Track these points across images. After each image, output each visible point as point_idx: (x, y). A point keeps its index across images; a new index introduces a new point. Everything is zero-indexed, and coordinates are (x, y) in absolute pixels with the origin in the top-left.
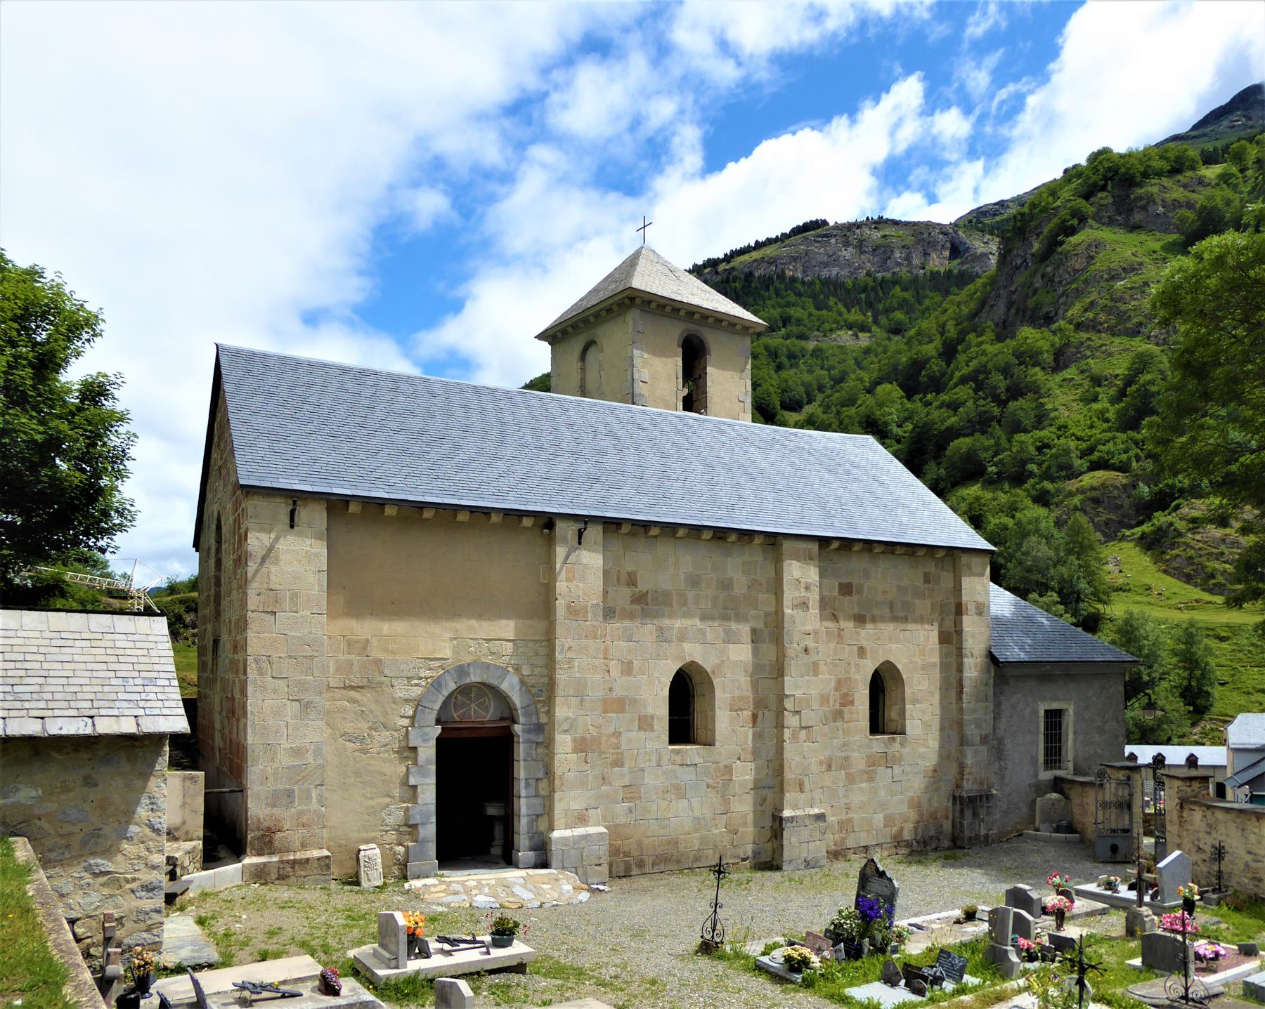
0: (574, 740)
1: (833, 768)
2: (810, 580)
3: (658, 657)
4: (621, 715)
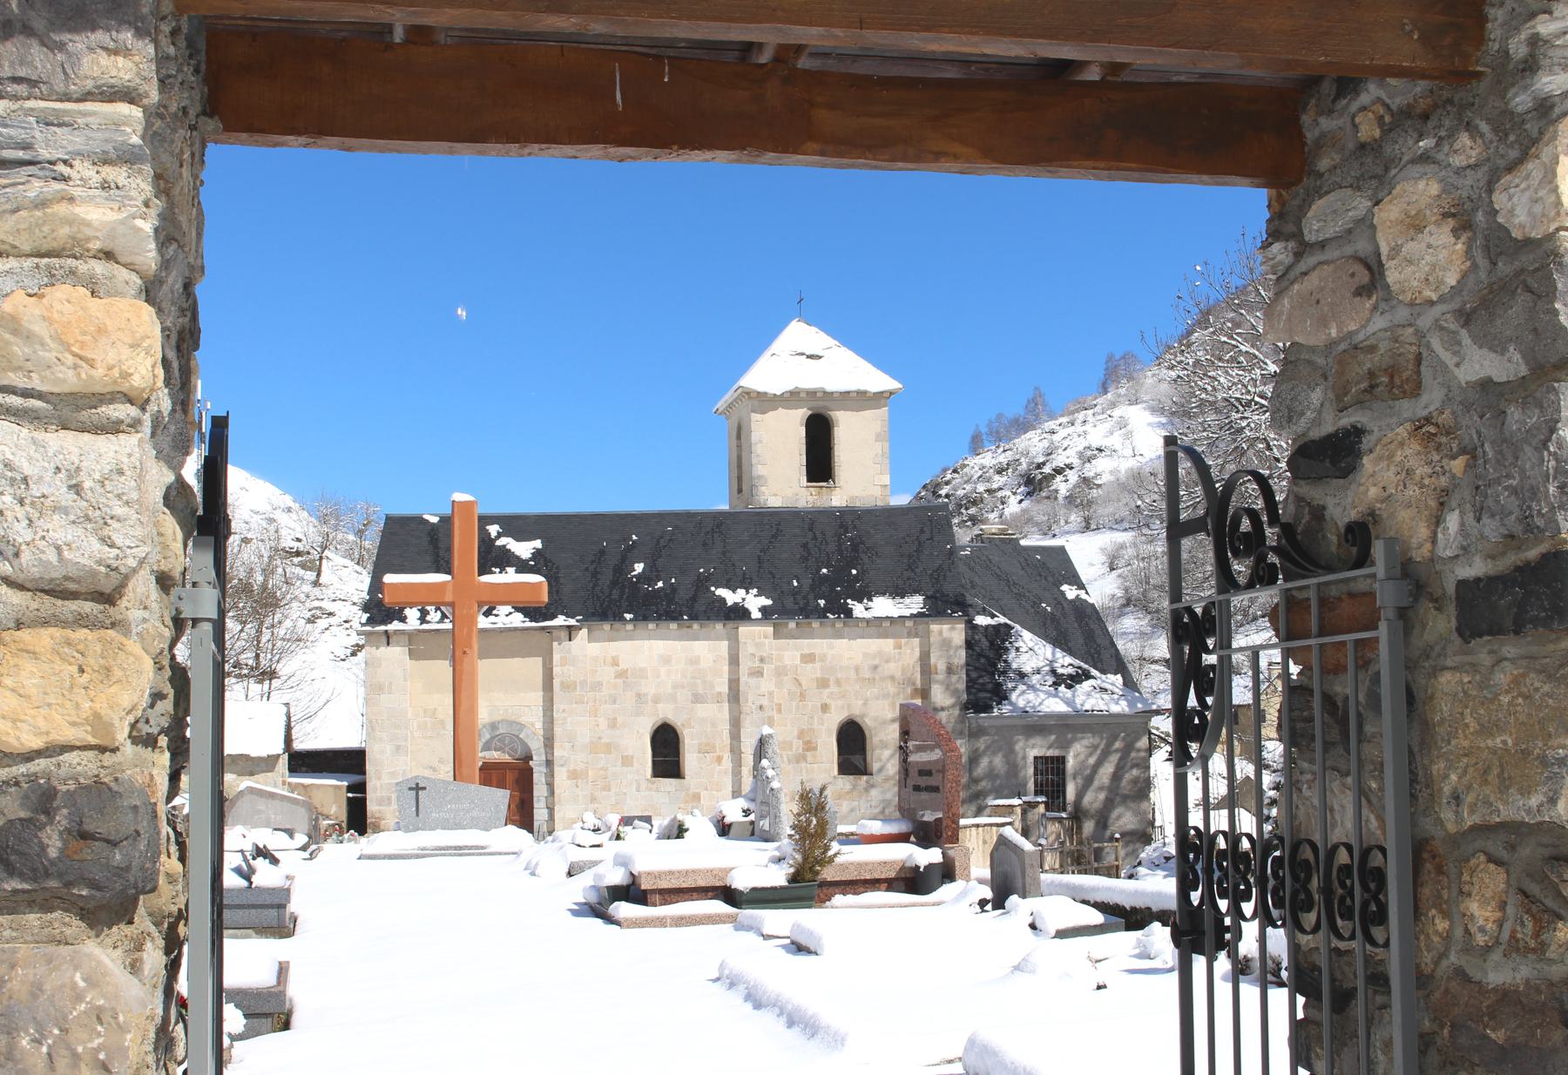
0: (568, 771)
3: (638, 714)
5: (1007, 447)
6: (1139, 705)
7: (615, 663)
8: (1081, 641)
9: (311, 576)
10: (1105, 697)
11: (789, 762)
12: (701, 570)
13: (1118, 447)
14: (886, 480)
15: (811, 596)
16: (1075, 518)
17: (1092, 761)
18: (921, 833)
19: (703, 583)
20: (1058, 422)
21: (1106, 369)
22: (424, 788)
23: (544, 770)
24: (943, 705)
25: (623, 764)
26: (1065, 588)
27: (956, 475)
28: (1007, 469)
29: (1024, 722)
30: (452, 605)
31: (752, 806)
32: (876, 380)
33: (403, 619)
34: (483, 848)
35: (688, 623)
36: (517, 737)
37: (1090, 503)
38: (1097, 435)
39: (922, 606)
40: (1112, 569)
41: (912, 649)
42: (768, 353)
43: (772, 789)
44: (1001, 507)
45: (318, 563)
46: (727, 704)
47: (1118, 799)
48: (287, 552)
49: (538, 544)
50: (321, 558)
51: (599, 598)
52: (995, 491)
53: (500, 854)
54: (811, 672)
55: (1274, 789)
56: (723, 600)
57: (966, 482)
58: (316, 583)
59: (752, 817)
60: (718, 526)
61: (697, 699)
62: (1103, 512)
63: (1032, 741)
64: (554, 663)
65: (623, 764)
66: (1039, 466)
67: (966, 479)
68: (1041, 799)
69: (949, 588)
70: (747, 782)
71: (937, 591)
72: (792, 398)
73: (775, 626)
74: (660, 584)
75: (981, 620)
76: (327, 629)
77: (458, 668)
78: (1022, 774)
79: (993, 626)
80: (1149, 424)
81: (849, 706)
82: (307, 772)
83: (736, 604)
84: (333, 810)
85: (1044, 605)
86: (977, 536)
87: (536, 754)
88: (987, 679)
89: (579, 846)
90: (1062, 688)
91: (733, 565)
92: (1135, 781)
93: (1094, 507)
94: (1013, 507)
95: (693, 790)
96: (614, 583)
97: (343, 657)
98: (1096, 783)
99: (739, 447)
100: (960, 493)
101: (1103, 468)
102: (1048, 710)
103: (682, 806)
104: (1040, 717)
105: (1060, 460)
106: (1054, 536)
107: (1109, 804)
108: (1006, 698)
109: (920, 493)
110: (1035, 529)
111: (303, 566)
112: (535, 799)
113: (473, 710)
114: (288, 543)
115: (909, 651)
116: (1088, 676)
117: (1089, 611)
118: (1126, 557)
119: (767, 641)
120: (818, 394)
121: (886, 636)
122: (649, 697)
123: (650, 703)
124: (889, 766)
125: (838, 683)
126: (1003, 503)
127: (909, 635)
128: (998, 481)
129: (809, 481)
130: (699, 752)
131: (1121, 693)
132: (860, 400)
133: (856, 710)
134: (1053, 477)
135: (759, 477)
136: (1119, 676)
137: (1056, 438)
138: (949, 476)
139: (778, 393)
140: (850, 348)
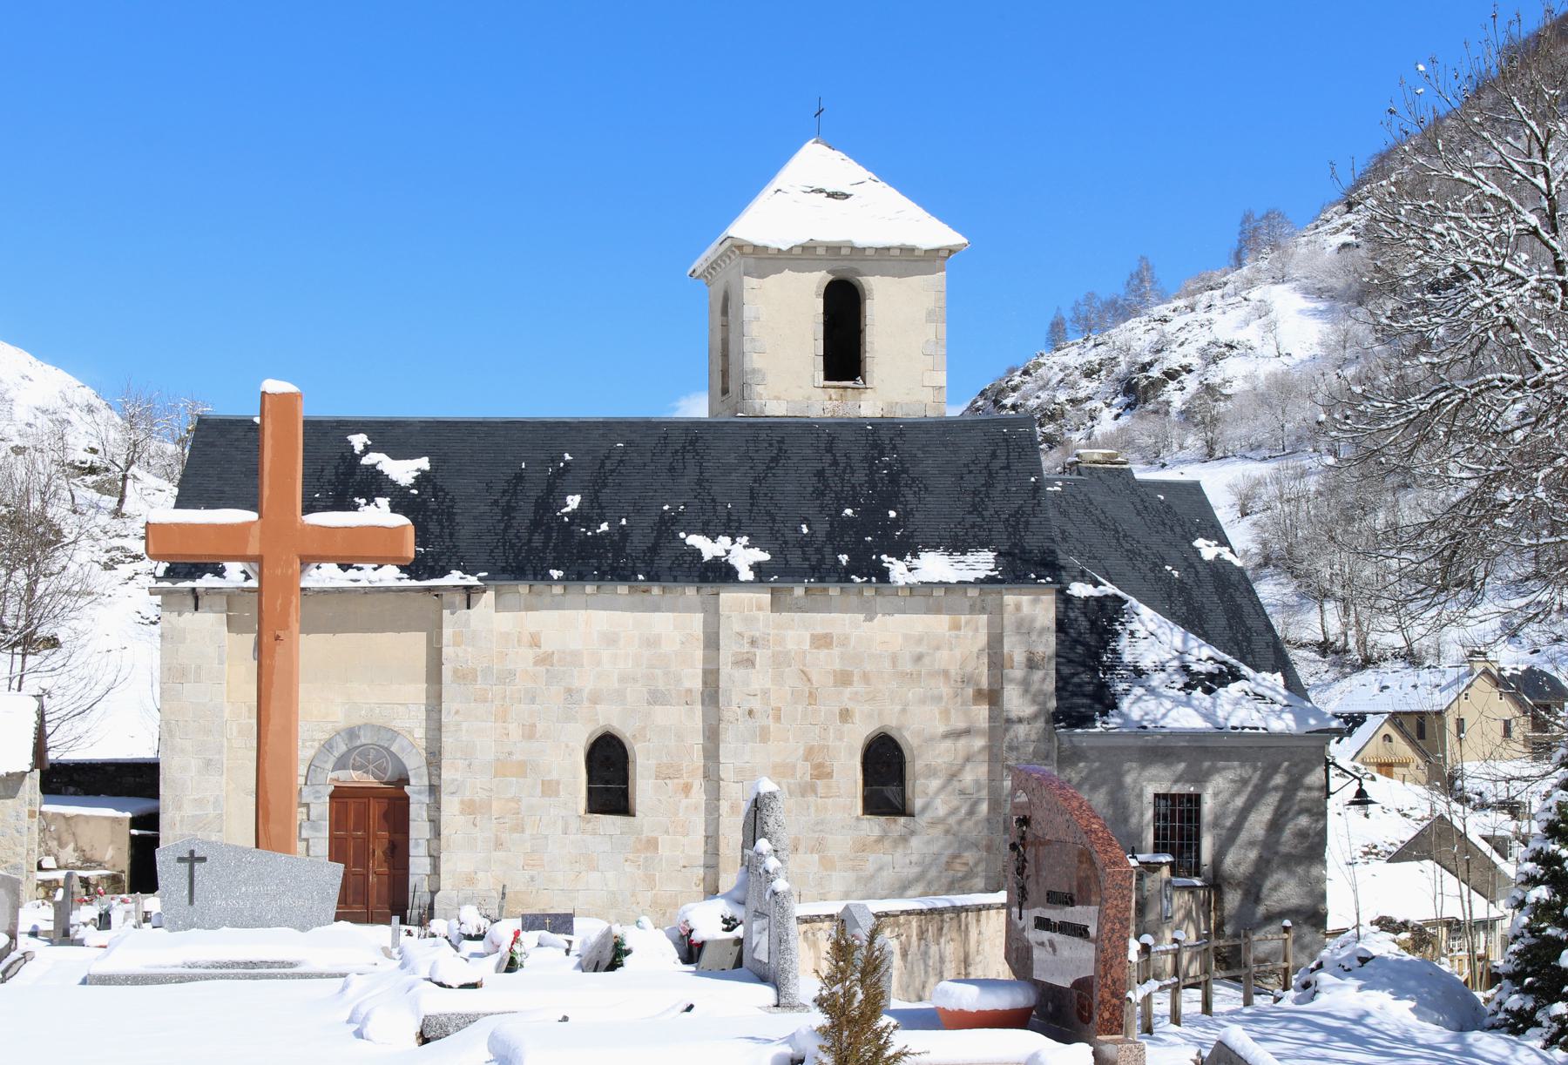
0: (462, 802)
1: (801, 849)
2: (757, 634)
4: (521, 780)
5: (1100, 340)
6: (1312, 722)
7: (535, 642)
8: (1223, 622)
9: (110, 502)
10: (1262, 707)
11: (791, 794)
12: (666, 508)
13: (1255, 343)
14: (941, 378)
15: (828, 549)
16: (1194, 441)
17: (1239, 802)
18: (1050, 1007)
19: (667, 527)
20: (1171, 307)
21: (1242, 233)
22: (203, 859)
23: (426, 799)
24: (1021, 714)
25: (544, 794)
26: (1200, 543)
27: (1028, 378)
28: (1099, 371)
29: (1140, 743)
30: (259, 559)
31: (739, 913)
32: (932, 233)
33: (219, 572)
34: (291, 965)
35: (644, 586)
36: (387, 749)
37: (1215, 421)
38: (1227, 324)
39: (992, 566)
40: (1244, 514)
41: (973, 633)
42: (769, 191)
43: (775, 893)
44: (1089, 424)
45: (120, 484)
46: (699, 707)
47: (1276, 860)
48: (76, 467)
49: (424, 463)
50: (125, 478)
51: (512, 546)
52: (1081, 401)
53: (320, 976)
54: (826, 662)
55: (1531, 860)
56: (697, 553)
57: (1042, 388)
58: (117, 513)
59: (739, 932)
60: (692, 443)
61: (656, 698)
62: (1233, 433)
63: (1146, 774)
64: (445, 641)
65: (544, 794)
66: (1145, 367)
67: (1041, 383)
68: (1166, 858)
69: (1032, 542)
70: (729, 879)
71: (1015, 545)
72: (804, 255)
73: (773, 592)
74: (604, 527)
75: (1079, 590)
76: (131, 579)
77: (266, 662)
78: (1134, 820)
79: (1097, 599)
80: (1301, 312)
81: (880, 714)
82: (75, 794)
83: (716, 558)
84: (108, 854)
85: (1169, 568)
86: (1071, 464)
87: (416, 775)
88: (1086, 677)
89: (441, 985)
90: (1198, 693)
91: (713, 500)
92: (1302, 834)
93: (1220, 426)
94: (1107, 424)
95: (647, 833)
96: (535, 525)
97: (154, 619)
98: (1243, 836)
99: (725, 326)
100: (1033, 403)
101: (1235, 373)
102: (1176, 725)
103: (631, 856)
104: (1164, 735)
105: (1173, 360)
106: (1164, 465)
107: (1262, 868)
108: (1115, 706)
109: (975, 402)
110: (1137, 456)
111: (100, 488)
112: (412, 843)
113: (289, 732)
114: (79, 455)
115: (971, 633)
116: (1236, 676)
117: (1235, 578)
118: (1265, 498)
119: (761, 614)
120: (844, 252)
121: (938, 610)
122: (585, 695)
123: (586, 704)
124: (938, 802)
125: (866, 678)
126: (1092, 418)
127: (973, 610)
128: (1086, 387)
129: (827, 378)
130: (657, 777)
131: (1285, 702)
132: (906, 260)
133: (888, 718)
134: (1164, 383)
135: (754, 371)
136: (1278, 675)
137: (1168, 328)
138: (1017, 380)
139: (784, 248)
140: (891, 184)
